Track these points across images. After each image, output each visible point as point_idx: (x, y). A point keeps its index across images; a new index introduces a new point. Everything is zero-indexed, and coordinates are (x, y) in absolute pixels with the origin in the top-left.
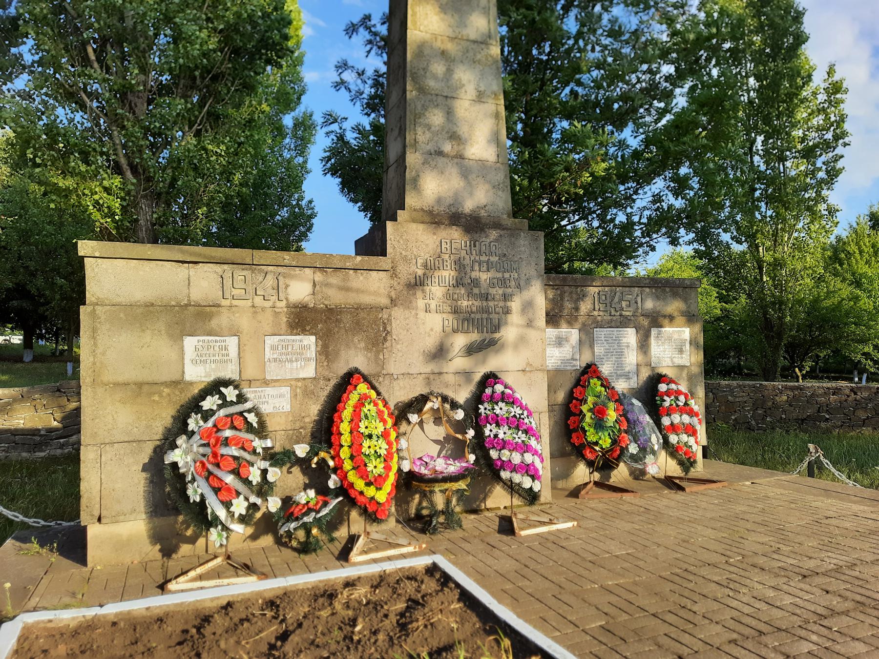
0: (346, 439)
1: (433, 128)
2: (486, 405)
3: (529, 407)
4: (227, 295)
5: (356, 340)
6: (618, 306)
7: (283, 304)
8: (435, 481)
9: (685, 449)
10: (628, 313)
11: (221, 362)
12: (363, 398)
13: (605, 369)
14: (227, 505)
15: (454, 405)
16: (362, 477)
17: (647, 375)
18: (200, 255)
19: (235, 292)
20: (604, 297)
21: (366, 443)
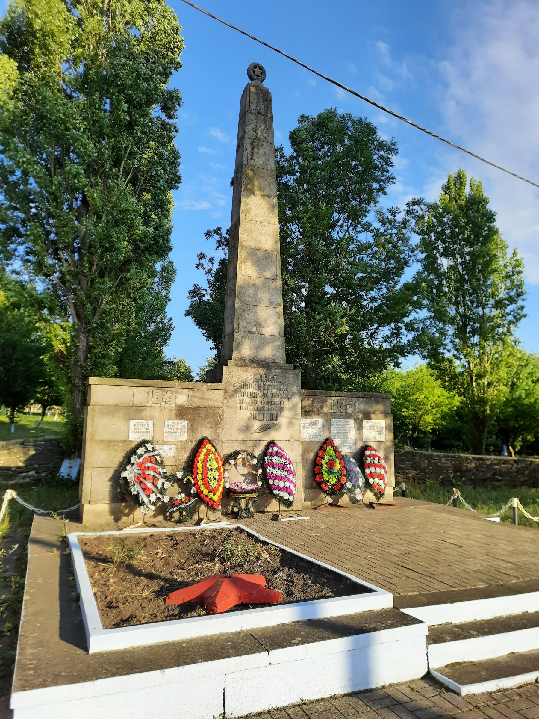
0: (200, 470)
1: (247, 321)
2: (268, 457)
3: (291, 460)
4: (150, 401)
5: (206, 423)
6: (344, 408)
7: (174, 405)
8: (241, 493)
9: (377, 486)
10: (350, 411)
11: (145, 432)
12: (209, 451)
13: (337, 442)
14: (148, 496)
15: (253, 457)
16: (207, 488)
17: (360, 446)
18: (139, 383)
19: (153, 400)
20: (336, 403)
21: (209, 473)
